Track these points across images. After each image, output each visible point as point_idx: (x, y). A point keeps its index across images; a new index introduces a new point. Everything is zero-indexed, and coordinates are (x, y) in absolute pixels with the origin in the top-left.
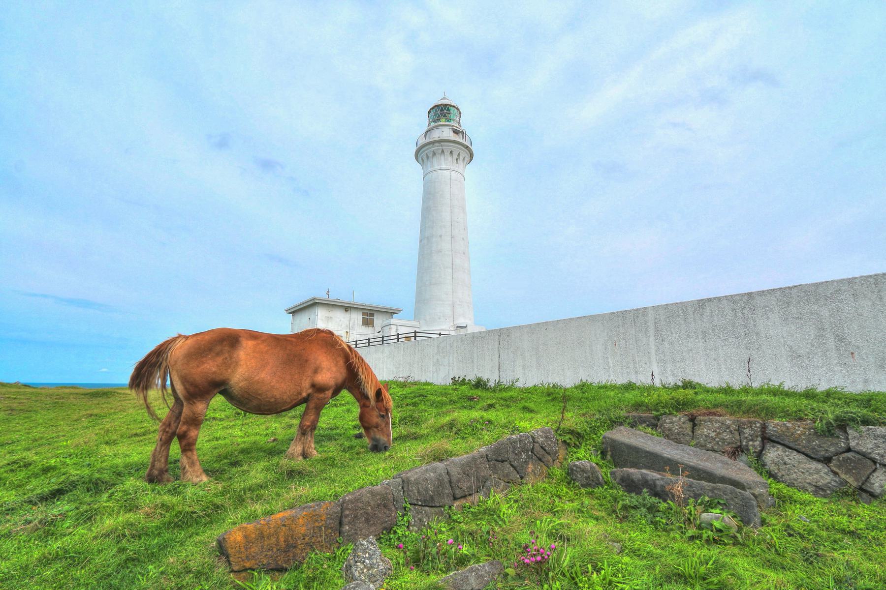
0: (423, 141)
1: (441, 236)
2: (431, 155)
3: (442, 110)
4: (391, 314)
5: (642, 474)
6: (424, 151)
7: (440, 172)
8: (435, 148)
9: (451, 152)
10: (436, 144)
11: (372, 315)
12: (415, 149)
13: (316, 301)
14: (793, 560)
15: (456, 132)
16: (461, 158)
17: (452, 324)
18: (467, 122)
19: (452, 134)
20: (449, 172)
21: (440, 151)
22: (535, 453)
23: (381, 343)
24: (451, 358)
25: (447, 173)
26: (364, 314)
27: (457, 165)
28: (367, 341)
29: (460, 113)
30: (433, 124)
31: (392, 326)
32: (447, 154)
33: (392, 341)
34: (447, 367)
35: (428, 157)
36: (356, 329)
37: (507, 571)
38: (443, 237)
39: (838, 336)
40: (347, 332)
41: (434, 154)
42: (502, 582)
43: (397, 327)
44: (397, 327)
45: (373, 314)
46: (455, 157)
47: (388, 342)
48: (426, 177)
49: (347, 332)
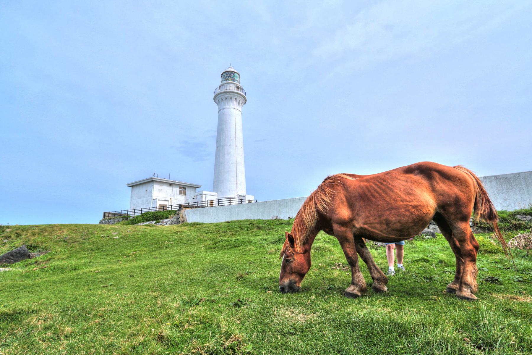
0: (218, 91)
1: (230, 145)
2: (224, 99)
3: (230, 74)
4: (195, 188)
5: (380, 284)
7: (229, 109)
8: (227, 95)
9: (236, 99)
10: (228, 94)
11: (185, 188)
12: (213, 95)
15: (238, 88)
16: (241, 103)
18: (243, 82)
20: (234, 110)
21: (230, 98)
23: (231, 199)
24: (287, 209)
26: (180, 188)
27: (239, 106)
29: (240, 77)
30: (225, 82)
31: (203, 195)
32: (233, 99)
33: (234, 200)
34: (285, 213)
35: (222, 100)
38: (231, 146)
39: (166, 247)
40: (171, 198)
41: (226, 98)
42: (63, 331)
45: (185, 188)
46: (238, 101)
49: (171, 198)
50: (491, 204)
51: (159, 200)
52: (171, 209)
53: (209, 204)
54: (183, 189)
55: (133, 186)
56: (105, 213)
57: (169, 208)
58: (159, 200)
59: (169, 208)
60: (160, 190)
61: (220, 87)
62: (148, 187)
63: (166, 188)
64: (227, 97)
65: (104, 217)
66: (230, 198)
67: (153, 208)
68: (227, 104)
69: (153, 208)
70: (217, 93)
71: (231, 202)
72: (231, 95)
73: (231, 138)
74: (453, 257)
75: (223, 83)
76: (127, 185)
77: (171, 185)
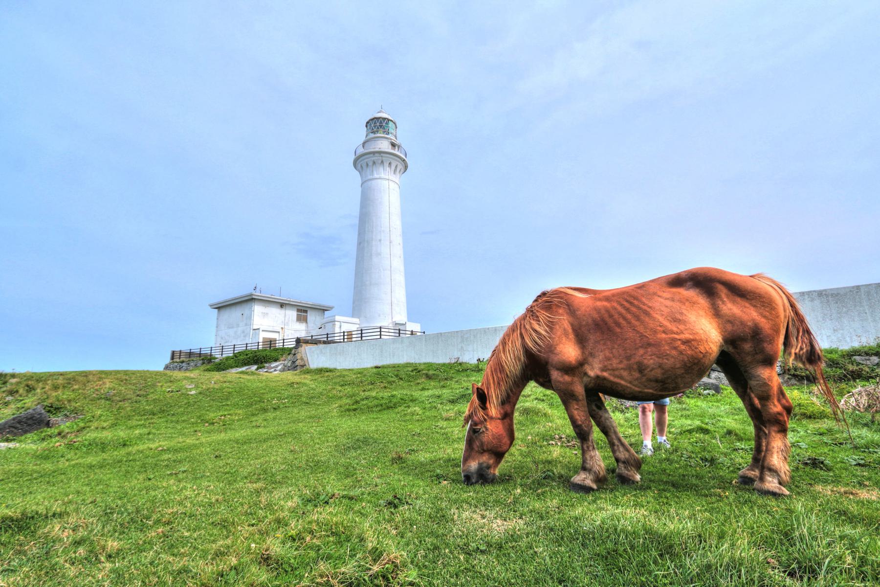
0: (361, 151)
1: (380, 240)
2: (370, 164)
4: (322, 311)
6: (364, 160)
7: (379, 181)
8: (376, 158)
9: (390, 164)
11: (306, 312)
12: (353, 157)
13: (254, 297)
14: (141, 516)
15: (393, 145)
16: (398, 170)
17: (390, 321)
18: (402, 135)
19: (390, 146)
20: (387, 182)
21: (380, 162)
22: (273, 443)
23: (382, 330)
25: (386, 182)
26: (298, 310)
27: (394, 176)
28: (326, 336)
29: (396, 128)
30: (372, 135)
31: (336, 323)
32: (386, 164)
33: (387, 330)
35: (367, 165)
36: (290, 325)
37: (688, 511)
40: (282, 328)
41: (374, 163)
43: (341, 324)
44: (341, 324)
46: (393, 167)
47: (292, 340)
48: (363, 186)
50: (812, 337)
51: (263, 331)
52: (283, 345)
53: (346, 337)
54: (303, 312)
55: (221, 307)
56: (173, 353)
57: (280, 344)
58: (263, 331)
59: (280, 344)
60: (265, 315)
61: (364, 144)
62: (244, 309)
63: (274, 311)
64: (375, 161)
65: (172, 358)
66: (381, 328)
67: (253, 345)
68: (375, 172)
69: (253, 345)
70: (358, 153)
71: (382, 333)
72: (382, 156)
73: (382, 229)
74: (749, 425)
75: (368, 137)
76: (211, 306)
77: (282, 305)
